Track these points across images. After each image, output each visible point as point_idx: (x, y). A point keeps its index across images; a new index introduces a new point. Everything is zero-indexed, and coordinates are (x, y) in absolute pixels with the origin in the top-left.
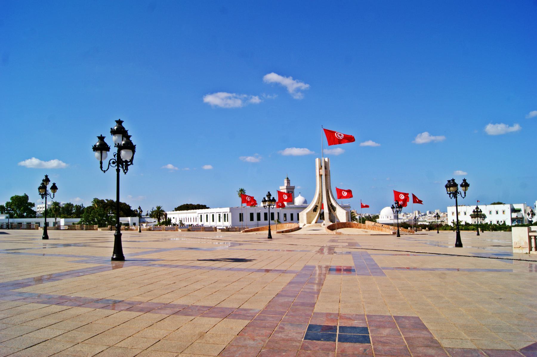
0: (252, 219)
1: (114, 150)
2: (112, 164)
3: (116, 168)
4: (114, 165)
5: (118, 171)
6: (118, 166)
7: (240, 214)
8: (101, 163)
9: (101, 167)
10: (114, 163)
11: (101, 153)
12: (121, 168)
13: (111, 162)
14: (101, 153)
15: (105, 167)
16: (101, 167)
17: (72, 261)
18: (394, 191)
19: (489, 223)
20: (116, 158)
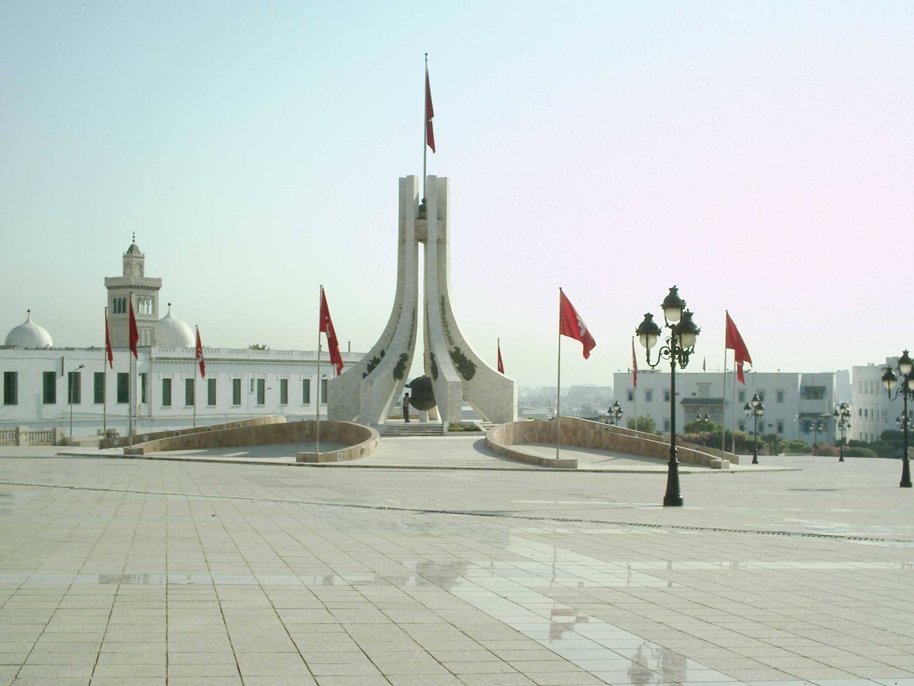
0: (50, 396)
1: (667, 333)
2: (664, 355)
3: (671, 360)
4: (667, 356)
5: (905, 399)
6: (673, 358)
7: (308, 402)
8: (648, 355)
9: (648, 361)
10: (666, 353)
11: (647, 339)
12: (677, 361)
13: (663, 351)
14: (647, 339)
15: (893, 397)
16: (648, 361)
17: (527, 559)
18: (674, 290)
19: (102, 438)
20: (670, 346)
